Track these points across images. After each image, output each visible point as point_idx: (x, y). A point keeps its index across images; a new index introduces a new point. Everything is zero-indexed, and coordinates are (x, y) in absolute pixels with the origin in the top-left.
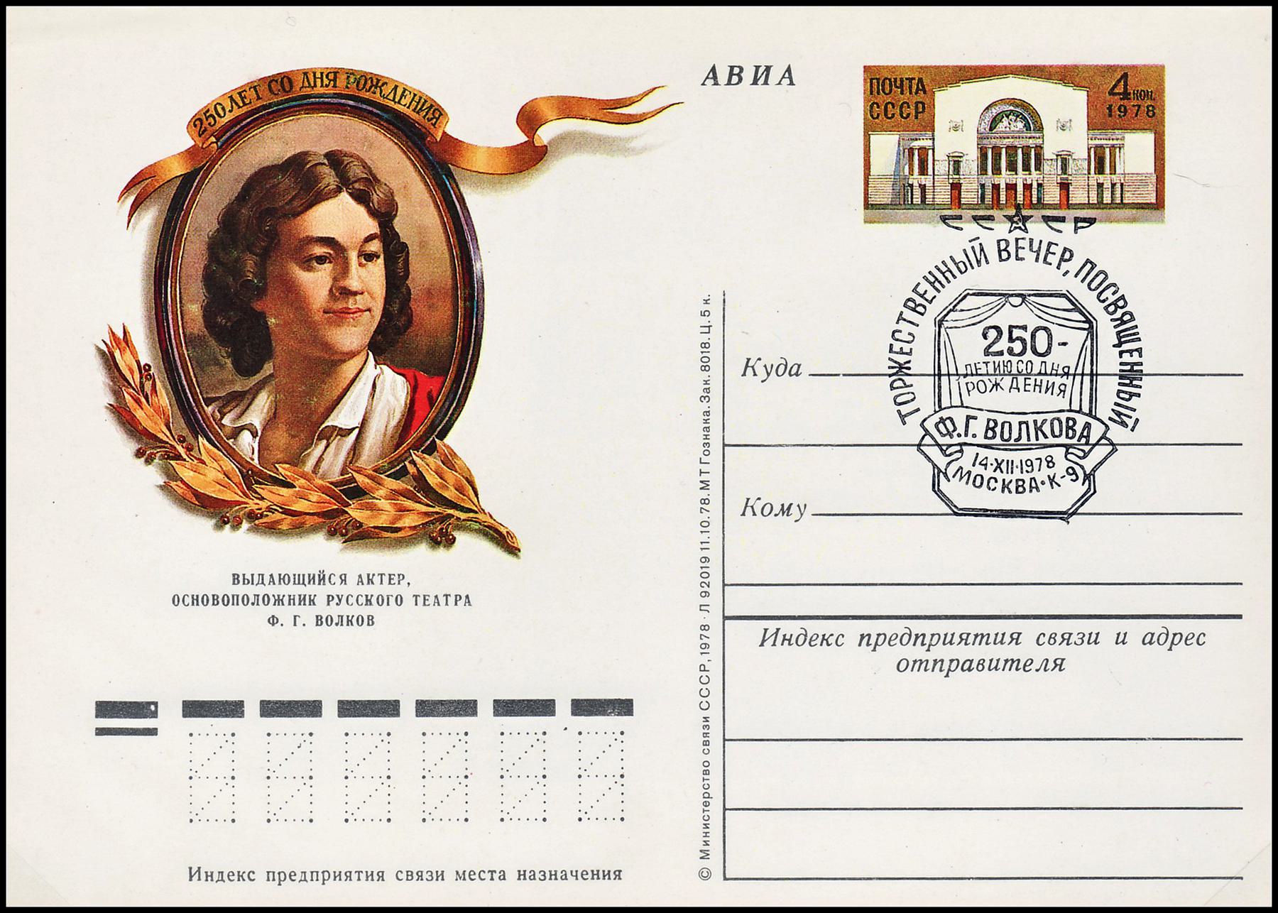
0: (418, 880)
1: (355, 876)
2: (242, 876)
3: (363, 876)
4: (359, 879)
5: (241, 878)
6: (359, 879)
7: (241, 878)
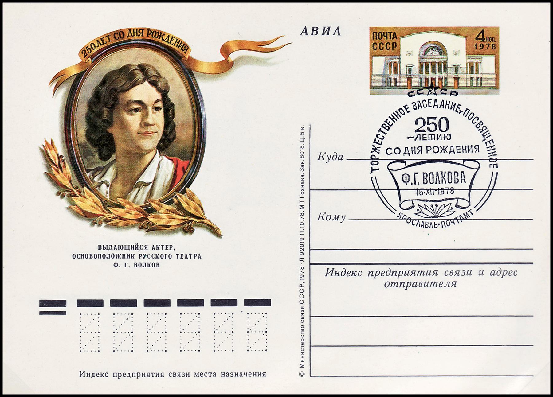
0: (263, 376)
1: (151, 375)
2: (102, 375)
3: (155, 375)
4: (153, 376)
5: (102, 376)
6: (153, 376)
7: (102, 376)
